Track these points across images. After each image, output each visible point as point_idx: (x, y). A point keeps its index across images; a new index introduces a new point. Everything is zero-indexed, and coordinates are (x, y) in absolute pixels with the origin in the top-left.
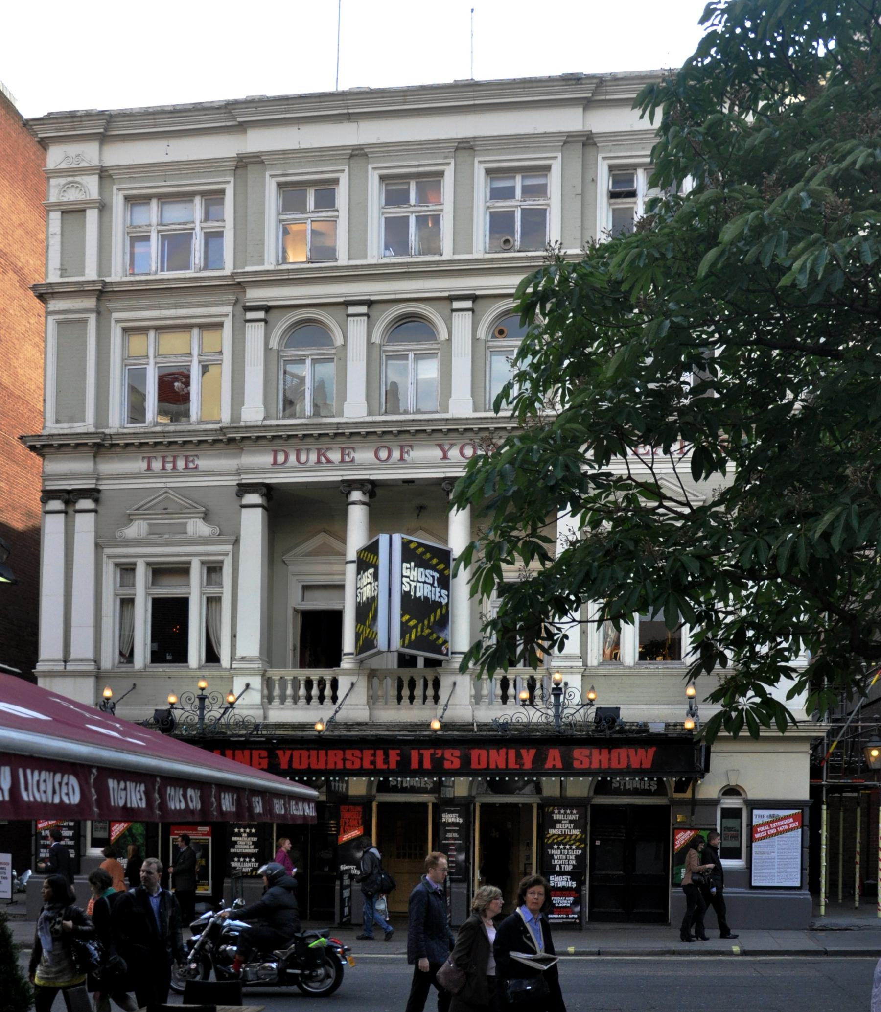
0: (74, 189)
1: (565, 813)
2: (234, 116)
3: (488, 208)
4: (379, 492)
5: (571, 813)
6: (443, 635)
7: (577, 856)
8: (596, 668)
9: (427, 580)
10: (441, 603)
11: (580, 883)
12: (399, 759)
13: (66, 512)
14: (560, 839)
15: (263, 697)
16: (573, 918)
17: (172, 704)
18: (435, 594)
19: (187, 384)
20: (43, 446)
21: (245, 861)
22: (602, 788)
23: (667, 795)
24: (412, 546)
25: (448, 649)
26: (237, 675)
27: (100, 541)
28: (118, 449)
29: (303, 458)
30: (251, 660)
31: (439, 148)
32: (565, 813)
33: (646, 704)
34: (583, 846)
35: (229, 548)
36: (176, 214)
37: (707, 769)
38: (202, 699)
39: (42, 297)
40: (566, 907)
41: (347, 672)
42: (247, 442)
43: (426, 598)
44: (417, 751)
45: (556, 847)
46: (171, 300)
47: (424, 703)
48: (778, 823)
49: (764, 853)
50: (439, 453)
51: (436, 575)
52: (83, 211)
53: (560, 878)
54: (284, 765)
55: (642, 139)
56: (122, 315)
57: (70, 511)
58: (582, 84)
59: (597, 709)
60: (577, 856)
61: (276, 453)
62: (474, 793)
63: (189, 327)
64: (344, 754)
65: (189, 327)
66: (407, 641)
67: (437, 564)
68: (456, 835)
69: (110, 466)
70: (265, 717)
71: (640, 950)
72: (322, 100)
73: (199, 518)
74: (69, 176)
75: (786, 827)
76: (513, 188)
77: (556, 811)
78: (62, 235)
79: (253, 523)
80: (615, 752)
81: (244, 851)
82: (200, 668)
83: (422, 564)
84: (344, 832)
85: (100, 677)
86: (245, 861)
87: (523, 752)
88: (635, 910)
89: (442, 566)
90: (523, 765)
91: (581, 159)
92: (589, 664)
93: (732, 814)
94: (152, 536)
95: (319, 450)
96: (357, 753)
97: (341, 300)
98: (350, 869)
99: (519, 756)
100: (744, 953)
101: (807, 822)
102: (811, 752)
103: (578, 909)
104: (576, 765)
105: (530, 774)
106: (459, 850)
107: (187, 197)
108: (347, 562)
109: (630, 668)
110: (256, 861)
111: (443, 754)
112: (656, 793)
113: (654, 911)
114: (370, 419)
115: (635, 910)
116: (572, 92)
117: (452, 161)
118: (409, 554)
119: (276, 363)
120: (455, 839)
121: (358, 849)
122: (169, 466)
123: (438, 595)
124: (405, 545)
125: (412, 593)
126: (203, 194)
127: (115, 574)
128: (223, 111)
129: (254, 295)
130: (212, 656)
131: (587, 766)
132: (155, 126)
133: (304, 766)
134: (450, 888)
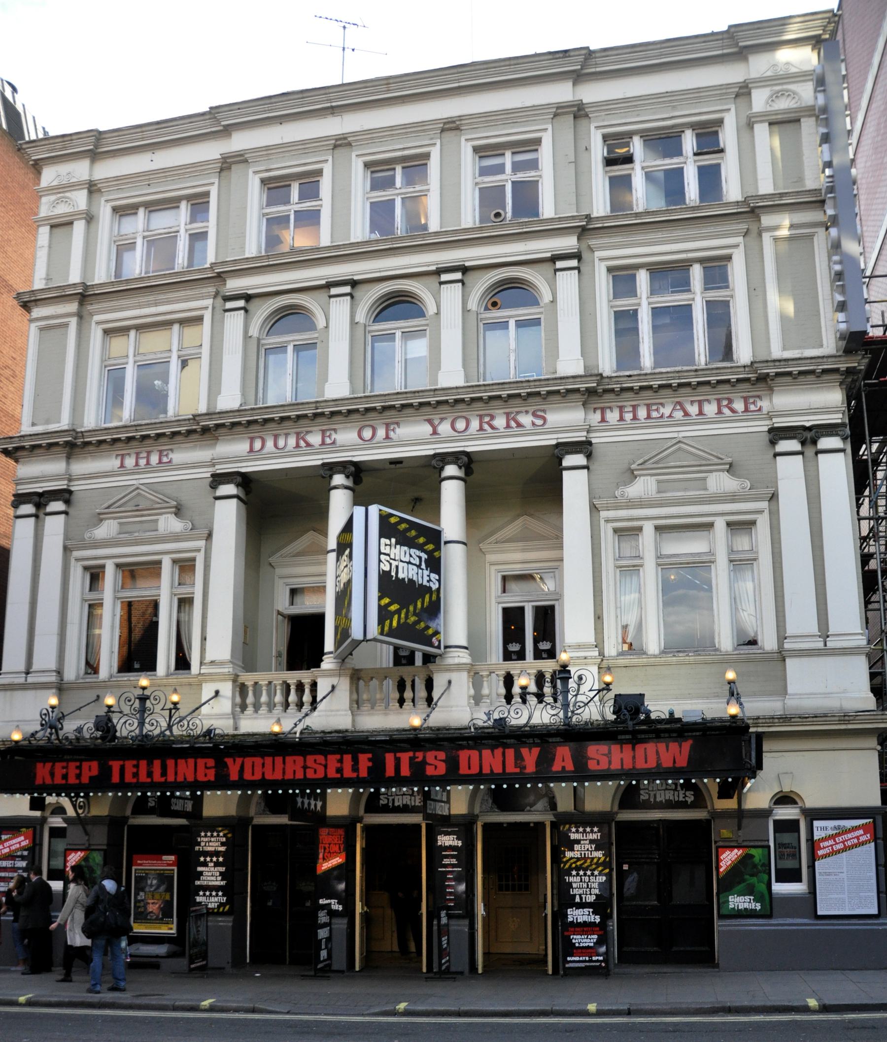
0: (63, 204)
1: (585, 831)
2: (219, 121)
3: (477, 184)
4: (366, 479)
5: (592, 831)
6: (433, 625)
7: (600, 884)
8: (614, 658)
9: (412, 560)
10: (430, 588)
11: (606, 917)
12: (370, 764)
13: (36, 516)
14: (578, 863)
15: (234, 705)
16: (597, 961)
17: (109, 707)
18: (424, 577)
19: (166, 381)
20: (17, 449)
21: (211, 895)
22: (629, 798)
23: (706, 807)
24: (393, 520)
25: (440, 641)
26: (206, 681)
27: (68, 543)
28: (91, 448)
29: (281, 443)
30: (222, 664)
31: (424, 131)
32: (585, 831)
33: (677, 699)
34: (607, 871)
35: (202, 543)
36: (162, 221)
37: (760, 766)
38: (143, 699)
39: (26, 306)
40: (588, 947)
41: (329, 673)
42: (222, 431)
43: (411, 581)
44: (392, 754)
45: (574, 873)
46: (151, 298)
47: (401, 706)
48: (845, 837)
49: (829, 874)
50: (427, 429)
51: (424, 556)
52: (71, 223)
53: (580, 912)
54: (234, 776)
55: (635, 106)
56: (104, 315)
57: (41, 515)
58: (569, 56)
59: (616, 696)
60: (600, 884)
61: (252, 440)
62: (477, 811)
63: (169, 324)
64: (305, 761)
65: (169, 324)
66: (386, 628)
67: (425, 544)
68: (454, 861)
69: (83, 466)
70: (236, 729)
71: (684, 1006)
72: (305, 95)
73: (722, 470)
74: (60, 193)
75: (856, 841)
76: (503, 165)
77: (574, 830)
78: (50, 247)
79: (227, 517)
80: (640, 748)
81: (210, 884)
82: (168, 675)
83: (404, 541)
84: (324, 859)
85: (61, 688)
86: (211, 895)
87: (525, 751)
88: (675, 949)
89: (430, 547)
90: (525, 768)
91: (572, 130)
92: (606, 654)
93: (787, 827)
94: (121, 536)
95: (298, 434)
96: (320, 758)
97: (323, 282)
98: (330, 904)
99: (519, 757)
100: (825, 1009)
101: (880, 834)
102: (879, 748)
103: (603, 949)
104: (592, 765)
105: (535, 780)
106: (458, 879)
107: (171, 204)
108: (328, 552)
109: (655, 656)
110: (223, 895)
111: (424, 757)
112: (694, 806)
113: (696, 949)
114: (352, 396)
115: (675, 949)
116: (560, 66)
117: (438, 142)
118: (387, 529)
119: (255, 350)
120: (453, 866)
121: (339, 879)
122: (143, 462)
123: (426, 578)
124: (384, 519)
125: (393, 574)
126: (188, 198)
127: (83, 578)
128: (207, 117)
129: (234, 285)
130: (182, 663)
131: (606, 767)
132: (143, 139)
133: (258, 777)
134: (447, 925)
